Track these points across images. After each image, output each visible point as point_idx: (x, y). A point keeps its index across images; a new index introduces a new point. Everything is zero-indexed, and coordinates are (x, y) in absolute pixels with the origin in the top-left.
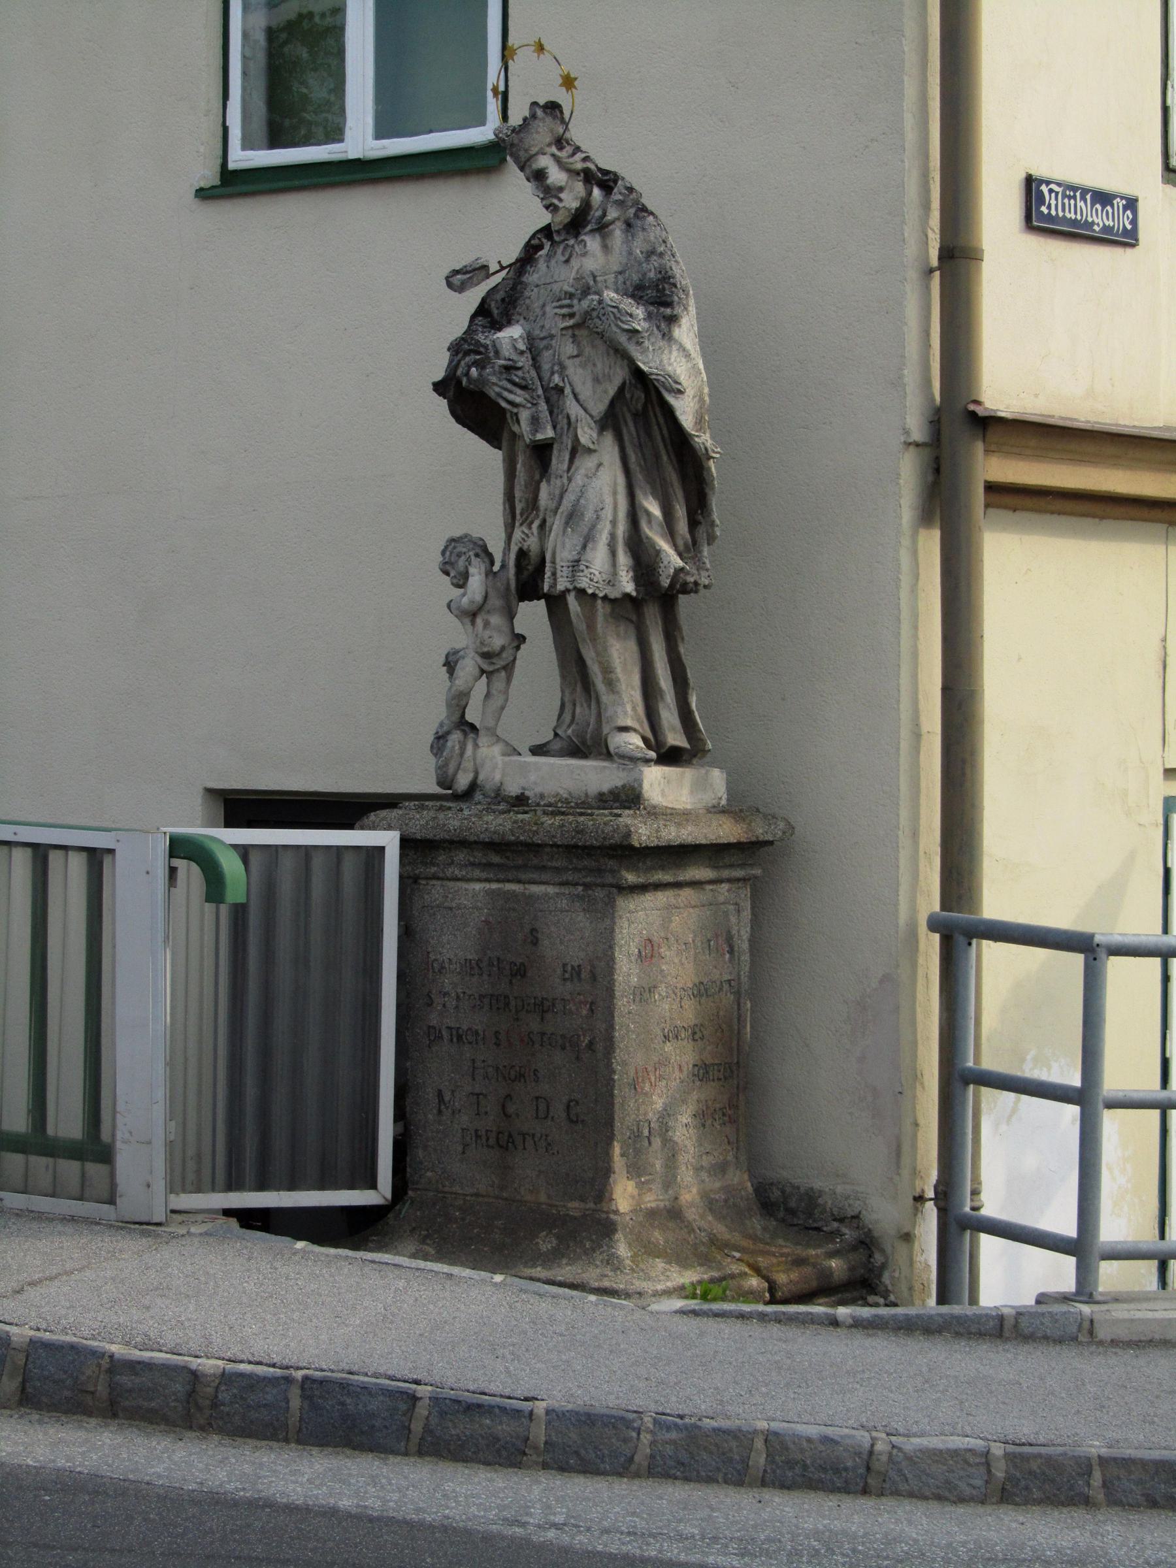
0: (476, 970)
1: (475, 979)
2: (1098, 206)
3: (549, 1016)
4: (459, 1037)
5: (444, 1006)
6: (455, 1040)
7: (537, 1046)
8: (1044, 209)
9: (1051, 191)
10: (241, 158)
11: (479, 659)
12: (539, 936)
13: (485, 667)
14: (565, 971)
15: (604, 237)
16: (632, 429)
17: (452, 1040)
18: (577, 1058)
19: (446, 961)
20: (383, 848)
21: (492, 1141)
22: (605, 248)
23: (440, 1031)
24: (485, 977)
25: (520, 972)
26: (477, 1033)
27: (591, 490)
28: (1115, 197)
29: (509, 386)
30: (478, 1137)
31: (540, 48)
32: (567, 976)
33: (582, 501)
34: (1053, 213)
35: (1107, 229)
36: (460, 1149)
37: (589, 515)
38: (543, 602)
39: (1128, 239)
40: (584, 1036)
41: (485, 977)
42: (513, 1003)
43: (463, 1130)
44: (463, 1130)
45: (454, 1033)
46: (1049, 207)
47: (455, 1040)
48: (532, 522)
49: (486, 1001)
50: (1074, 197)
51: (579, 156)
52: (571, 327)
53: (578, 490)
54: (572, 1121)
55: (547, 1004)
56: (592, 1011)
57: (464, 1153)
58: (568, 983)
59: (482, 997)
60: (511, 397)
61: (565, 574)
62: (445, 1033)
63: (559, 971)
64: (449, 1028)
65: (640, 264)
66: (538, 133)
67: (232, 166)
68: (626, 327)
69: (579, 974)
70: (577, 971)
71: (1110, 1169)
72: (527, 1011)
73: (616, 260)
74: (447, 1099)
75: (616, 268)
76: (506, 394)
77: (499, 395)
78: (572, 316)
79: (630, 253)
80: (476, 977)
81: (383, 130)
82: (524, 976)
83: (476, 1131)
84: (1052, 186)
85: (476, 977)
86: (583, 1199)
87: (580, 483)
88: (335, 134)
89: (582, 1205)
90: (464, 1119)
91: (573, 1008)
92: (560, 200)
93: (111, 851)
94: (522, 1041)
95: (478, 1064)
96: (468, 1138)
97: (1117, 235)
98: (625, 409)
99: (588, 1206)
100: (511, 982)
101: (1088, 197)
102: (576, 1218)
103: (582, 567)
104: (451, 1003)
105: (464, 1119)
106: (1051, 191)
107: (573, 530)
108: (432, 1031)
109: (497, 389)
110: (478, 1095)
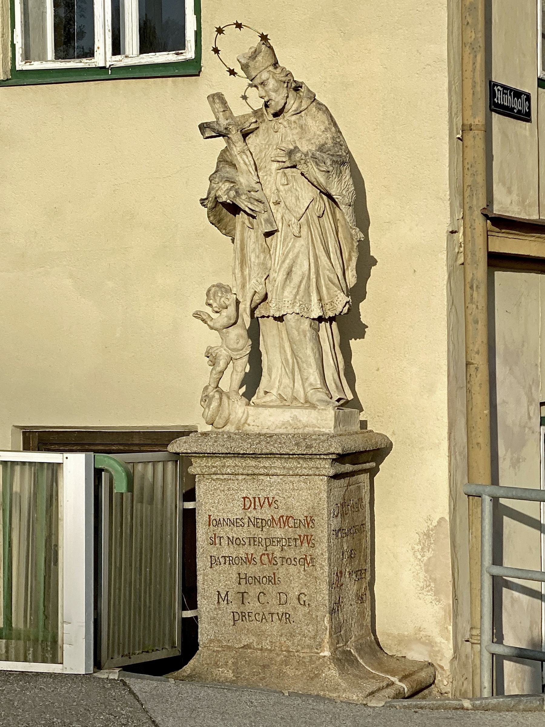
2: (516, 99)
8: (496, 100)
9: (498, 90)
10: (20, 65)
28: (523, 94)
31: (220, 31)
34: (499, 102)
35: (519, 112)
39: (525, 117)
46: (498, 99)
50: (507, 94)
66: (377, 443)
67: (18, 68)
71: (506, 610)
81: (144, 49)
84: (499, 87)
88: (91, 54)
93: (59, 464)
95: (243, 576)
97: (523, 115)
101: (512, 93)
106: (498, 90)
110: (243, 593)
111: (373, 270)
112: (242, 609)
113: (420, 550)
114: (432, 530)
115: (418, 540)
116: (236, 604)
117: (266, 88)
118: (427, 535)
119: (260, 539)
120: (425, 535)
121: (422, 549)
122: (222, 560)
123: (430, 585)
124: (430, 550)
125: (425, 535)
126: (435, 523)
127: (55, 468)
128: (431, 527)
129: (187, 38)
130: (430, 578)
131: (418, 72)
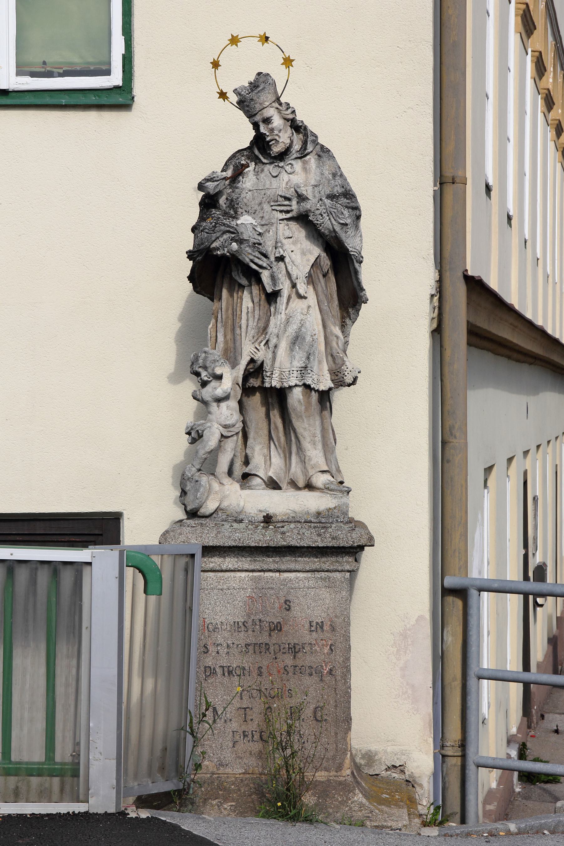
0: (243, 628)
1: (242, 634)
3: (300, 655)
4: (230, 673)
5: (218, 653)
6: (226, 674)
7: (290, 674)
11: (221, 428)
12: (291, 604)
13: (225, 434)
14: (311, 626)
15: (305, 163)
16: (323, 284)
17: (224, 675)
18: (321, 680)
19: (219, 623)
20: (203, 547)
21: (257, 737)
22: (305, 169)
23: (214, 669)
24: (250, 632)
25: (277, 628)
26: (244, 669)
27: (308, 323)
29: (260, 256)
30: (245, 736)
32: (313, 629)
33: (303, 329)
36: (231, 745)
37: (308, 339)
38: (258, 394)
40: (326, 666)
41: (250, 632)
42: (272, 648)
43: (233, 732)
44: (233, 732)
45: (226, 669)
47: (226, 674)
48: (261, 342)
49: (251, 648)
51: (290, 111)
52: (286, 219)
53: (298, 322)
54: (317, 720)
55: (297, 647)
56: (332, 650)
57: (234, 747)
58: (314, 633)
59: (247, 645)
60: (260, 263)
61: (295, 375)
62: (219, 671)
63: (307, 626)
64: (223, 667)
65: (329, 180)
68: (342, 222)
69: (322, 627)
70: (321, 626)
72: (284, 653)
73: (313, 179)
74: (219, 713)
75: (313, 182)
76: (256, 260)
77: (252, 261)
78: (287, 212)
79: (322, 174)
80: (243, 633)
82: (280, 630)
83: (244, 732)
85: (243, 633)
86: (326, 769)
87: (299, 318)
88: (108, 73)
89: (327, 773)
90: (234, 725)
91: (318, 649)
92: (279, 137)
94: (279, 672)
96: (238, 738)
98: (319, 271)
99: (331, 774)
100: (270, 635)
102: (323, 782)
103: (309, 371)
104: (223, 651)
105: (234, 725)
107: (299, 348)
108: (208, 670)
109: (252, 257)
111: (188, 274)
112: (244, 728)
113: (395, 653)
114: (409, 630)
115: (393, 642)
116: (237, 722)
117: (270, 126)
118: (404, 636)
119: (277, 646)
120: (402, 635)
121: (398, 651)
122: (219, 671)
123: (406, 692)
124: (408, 652)
125: (402, 635)
126: (413, 622)
127: (78, 567)
128: (408, 626)
129: (497, 216)
130: (407, 684)
131: (398, 116)
